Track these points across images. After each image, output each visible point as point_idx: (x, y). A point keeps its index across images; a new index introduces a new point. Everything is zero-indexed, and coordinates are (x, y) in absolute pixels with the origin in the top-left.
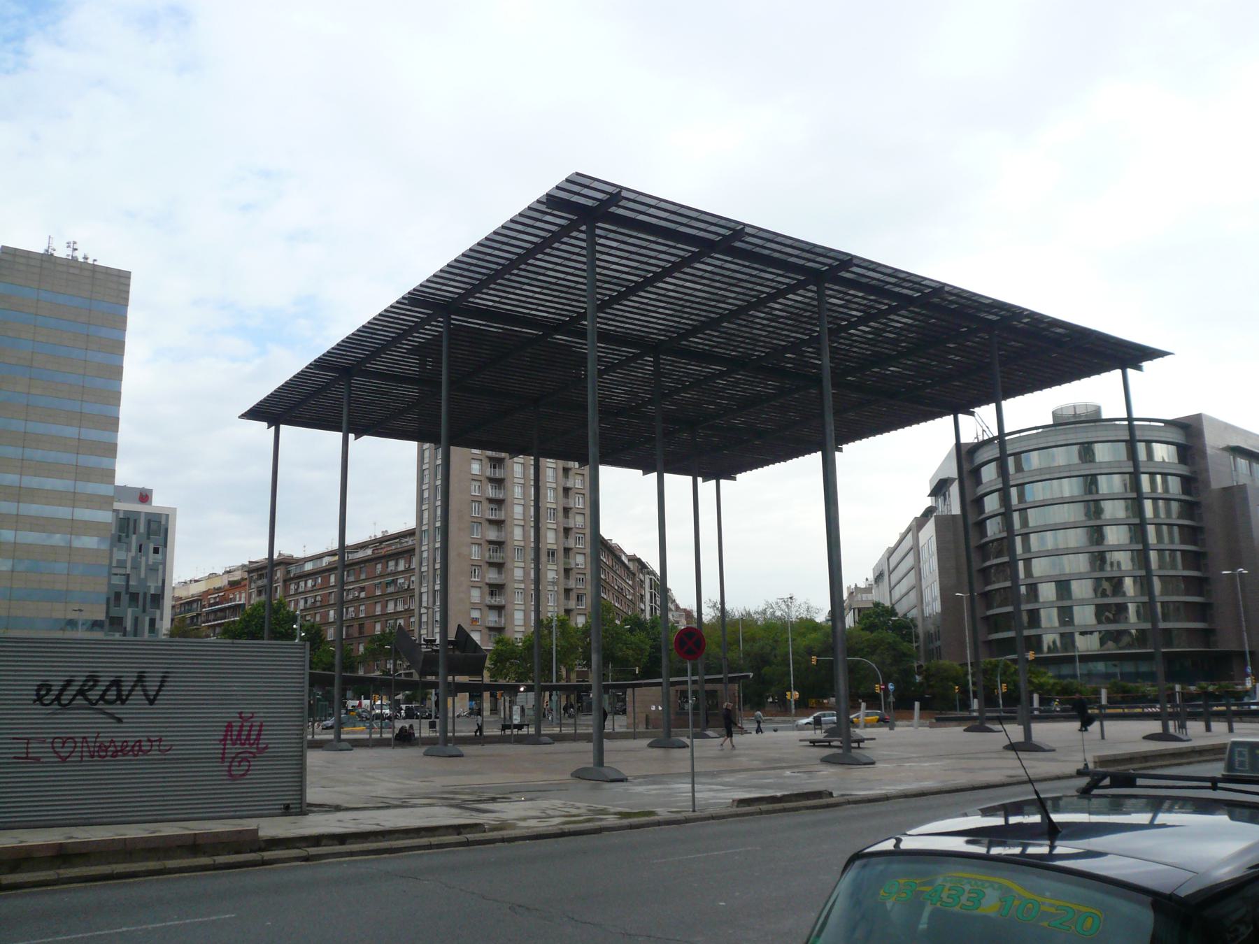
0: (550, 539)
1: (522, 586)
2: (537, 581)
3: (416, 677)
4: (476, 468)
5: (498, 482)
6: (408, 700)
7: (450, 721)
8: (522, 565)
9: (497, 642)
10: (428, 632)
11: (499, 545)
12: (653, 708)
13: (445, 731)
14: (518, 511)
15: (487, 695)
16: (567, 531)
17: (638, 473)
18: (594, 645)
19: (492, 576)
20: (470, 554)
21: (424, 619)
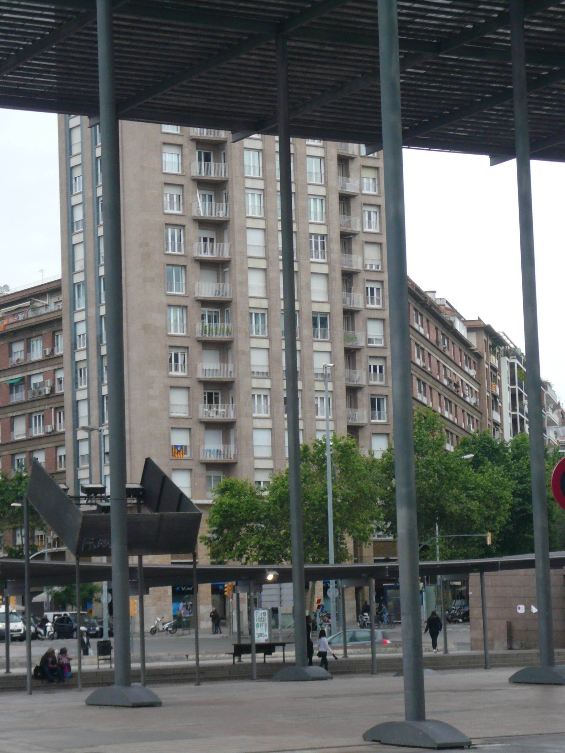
0: (317, 293)
1: (267, 383)
2: (292, 374)
3: (71, 560)
4: (171, 161)
5: (215, 188)
6: (59, 603)
7: (136, 640)
8: (265, 343)
9: (223, 491)
10: (88, 471)
11: (220, 307)
12: (521, 609)
13: (126, 659)
14: (255, 242)
15: (205, 589)
16: (348, 277)
17: (482, 160)
18: (401, 492)
19: (210, 366)
20: (167, 328)
21: (84, 449)
